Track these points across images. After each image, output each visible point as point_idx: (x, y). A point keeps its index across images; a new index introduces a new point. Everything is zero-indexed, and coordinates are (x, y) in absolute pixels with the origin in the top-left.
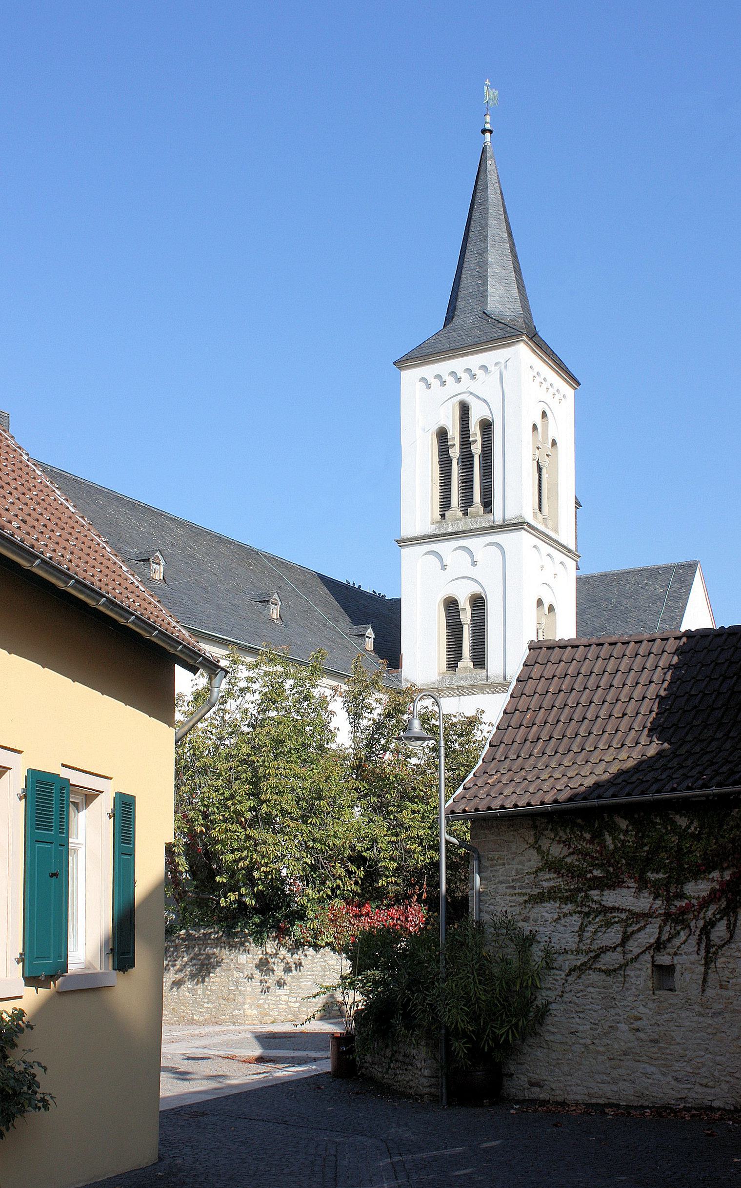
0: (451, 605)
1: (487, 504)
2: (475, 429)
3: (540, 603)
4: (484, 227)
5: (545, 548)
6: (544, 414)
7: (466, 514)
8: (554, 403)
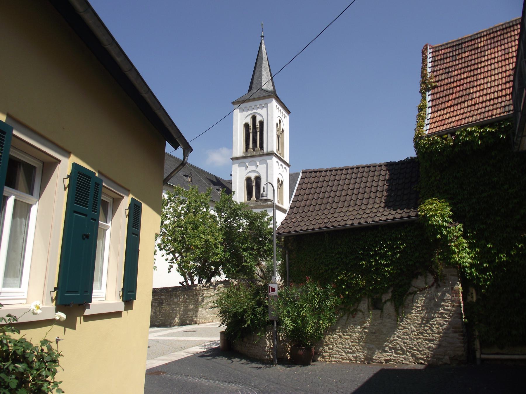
0: (248, 180)
1: (262, 147)
2: (257, 123)
3: (278, 180)
4: (261, 64)
5: (280, 163)
6: (280, 120)
7: (254, 150)
8: (283, 118)
